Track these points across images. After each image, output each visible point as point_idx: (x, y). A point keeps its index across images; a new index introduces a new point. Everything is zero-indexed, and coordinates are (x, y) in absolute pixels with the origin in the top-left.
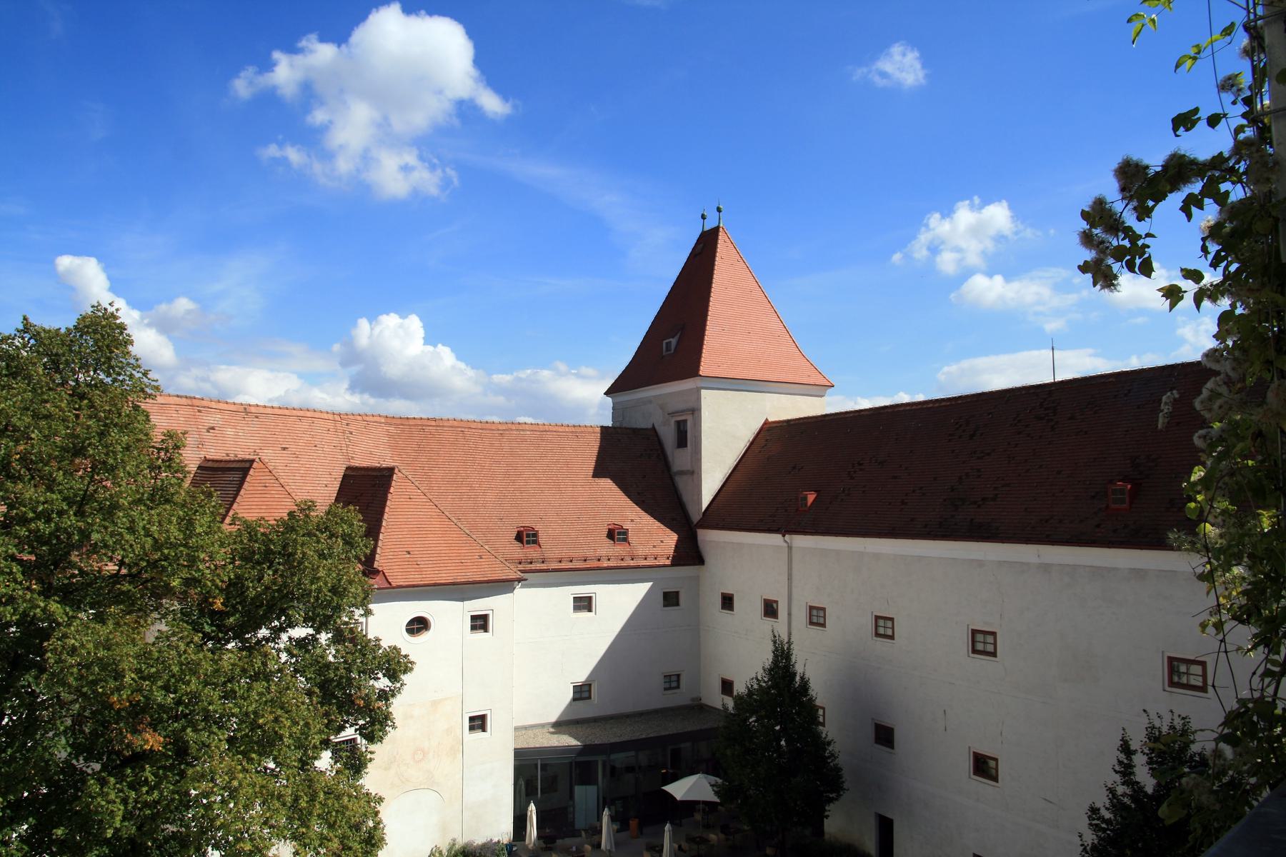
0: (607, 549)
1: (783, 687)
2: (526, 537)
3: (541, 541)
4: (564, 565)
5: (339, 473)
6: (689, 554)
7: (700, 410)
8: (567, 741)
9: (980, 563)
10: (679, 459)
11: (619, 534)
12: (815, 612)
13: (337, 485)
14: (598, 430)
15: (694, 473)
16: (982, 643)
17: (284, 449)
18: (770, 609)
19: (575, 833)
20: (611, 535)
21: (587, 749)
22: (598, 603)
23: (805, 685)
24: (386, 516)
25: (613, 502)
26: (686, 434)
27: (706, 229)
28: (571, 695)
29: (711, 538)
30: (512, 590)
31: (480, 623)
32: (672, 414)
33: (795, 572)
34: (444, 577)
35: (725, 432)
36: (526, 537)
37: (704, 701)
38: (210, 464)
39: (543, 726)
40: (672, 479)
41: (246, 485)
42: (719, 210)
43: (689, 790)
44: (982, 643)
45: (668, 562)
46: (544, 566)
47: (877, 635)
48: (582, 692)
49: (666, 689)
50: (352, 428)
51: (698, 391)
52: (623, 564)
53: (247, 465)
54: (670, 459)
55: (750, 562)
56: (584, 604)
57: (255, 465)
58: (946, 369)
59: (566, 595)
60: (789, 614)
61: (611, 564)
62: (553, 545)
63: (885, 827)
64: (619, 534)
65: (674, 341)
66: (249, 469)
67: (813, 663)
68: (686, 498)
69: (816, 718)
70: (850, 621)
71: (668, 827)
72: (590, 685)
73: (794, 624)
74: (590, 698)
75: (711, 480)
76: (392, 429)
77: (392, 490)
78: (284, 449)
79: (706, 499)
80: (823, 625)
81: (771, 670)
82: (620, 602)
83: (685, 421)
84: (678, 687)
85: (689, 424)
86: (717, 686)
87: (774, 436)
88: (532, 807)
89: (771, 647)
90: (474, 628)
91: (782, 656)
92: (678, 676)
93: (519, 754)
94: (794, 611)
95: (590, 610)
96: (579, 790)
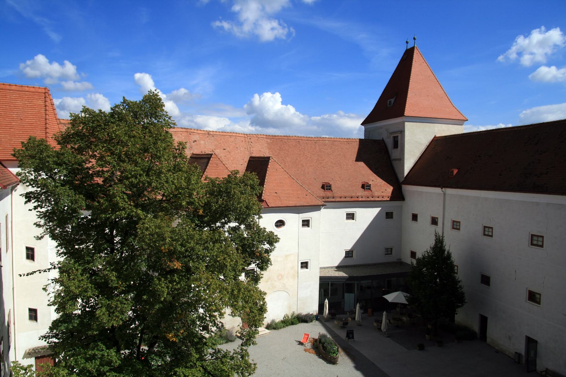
0: (362, 193)
1: (439, 255)
2: (326, 187)
3: (333, 189)
4: (342, 199)
5: (247, 159)
6: (398, 195)
8: (341, 274)
9: (537, 204)
10: (394, 154)
11: (367, 186)
14: (358, 140)
15: (401, 160)
17: (224, 149)
18: (434, 221)
19: (344, 313)
20: (363, 187)
21: (350, 278)
22: (357, 216)
23: (449, 255)
24: (266, 177)
25: (364, 172)
26: (398, 141)
27: (409, 48)
29: (408, 189)
30: (319, 210)
31: (306, 223)
33: (446, 205)
34: (291, 203)
35: (416, 141)
36: (326, 187)
38: (194, 156)
39: (332, 267)
40: (391, 163)
41: (209, 164)
42: (414, 39)
45: (388, 199)
46: (333, 200)
47: (484, 235)
48: (349, 254)
49: (386, 254)
50: (252, 140)
55: (426, 200)
56: (351, 216)
57: (213, 156)
59: (343, 212)
60: (443, 224)
61: (363, 199)
62: (338, 191)
63: (484, 321)
64: (367, 186)
65: (393, 100)
66: (210, 158)
67: (454, 246)
68: (397, 171)
70: (471, 227)
71: (385, 313)
75: (409, 164)
76: (269, 140)
77: (269, 166)
78: (224, 149)
79: (407, 171)
80: (459, 229)
81: (434, 248)
82: (366, 216)
83: (397, 137)
84: (391, 254)
85: (399, 138)
86: (409, 254)
87: (438, 144)
88: (327, 301)
89: (434, 238)
90: (303, 225)
93: (321, 278)
94: (445, 223)
95: (353, 219)
96: (346, 295)
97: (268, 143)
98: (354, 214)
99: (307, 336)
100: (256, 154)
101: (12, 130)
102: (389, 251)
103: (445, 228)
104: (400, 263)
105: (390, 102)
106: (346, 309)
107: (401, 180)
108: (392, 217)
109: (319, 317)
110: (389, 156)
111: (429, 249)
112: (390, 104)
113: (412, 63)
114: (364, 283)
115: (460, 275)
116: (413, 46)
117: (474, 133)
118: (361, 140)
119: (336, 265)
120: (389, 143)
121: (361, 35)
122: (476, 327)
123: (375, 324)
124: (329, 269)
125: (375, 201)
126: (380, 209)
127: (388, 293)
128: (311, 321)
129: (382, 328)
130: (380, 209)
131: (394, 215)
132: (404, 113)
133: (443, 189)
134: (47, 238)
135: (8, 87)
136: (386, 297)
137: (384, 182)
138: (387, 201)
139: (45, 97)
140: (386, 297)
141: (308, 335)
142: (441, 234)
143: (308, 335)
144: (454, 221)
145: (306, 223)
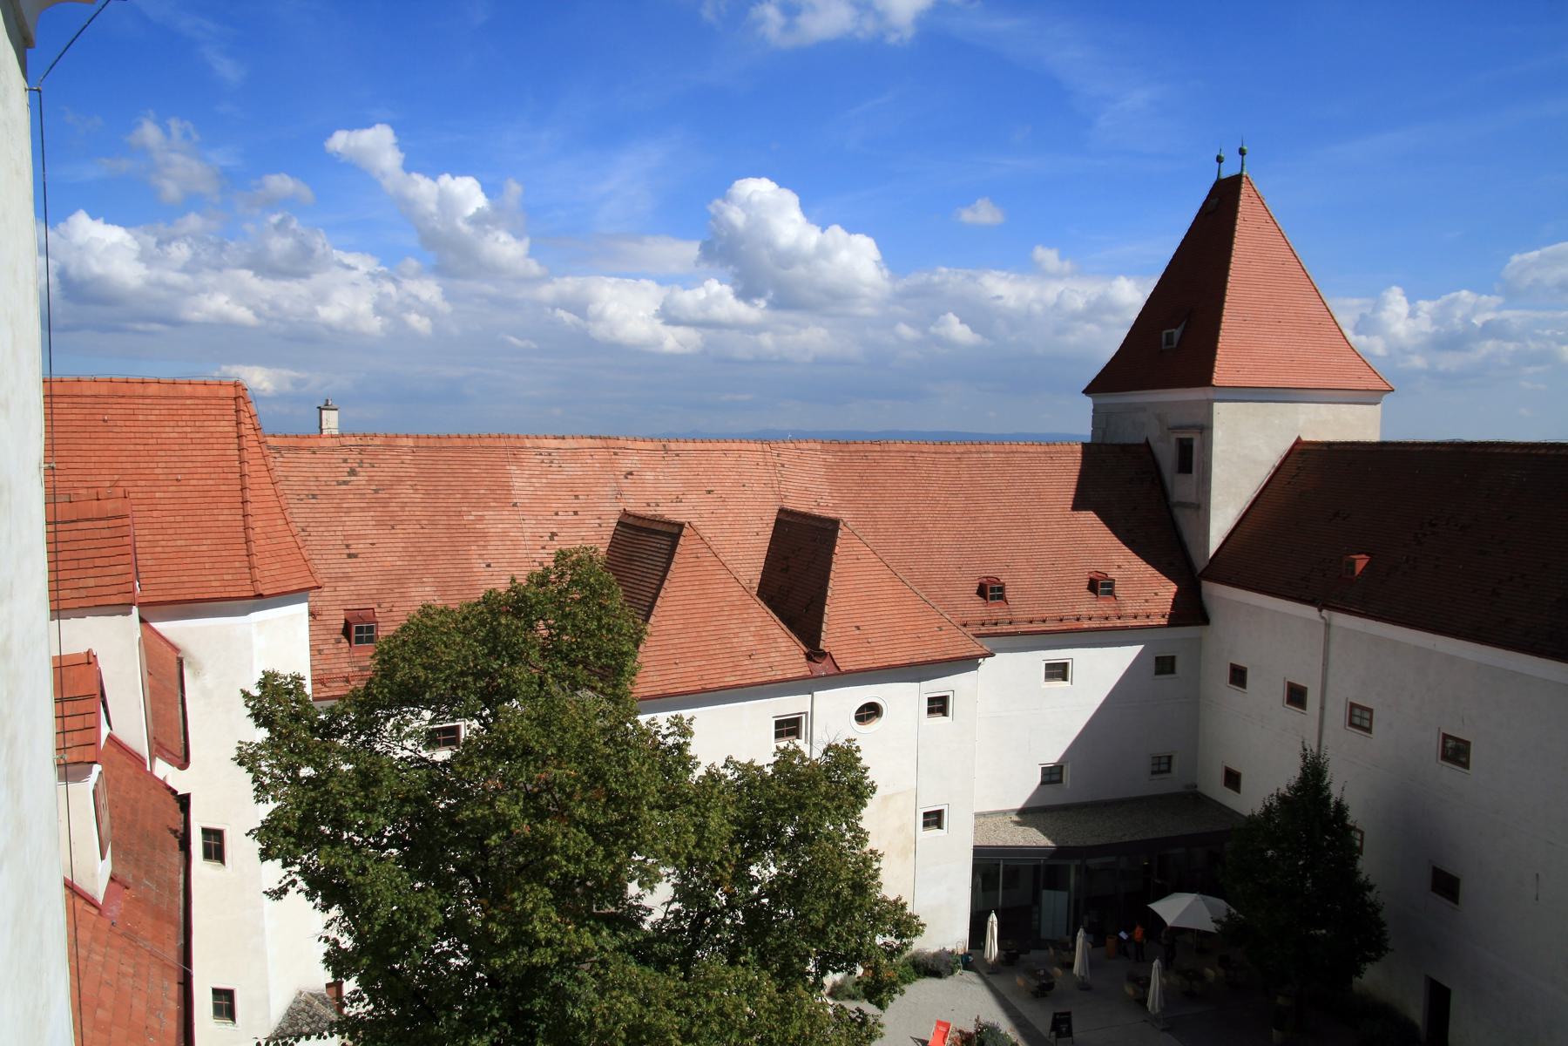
0: (1089, 608)
1: (1310, 803)
2: (990, 591)
3: (1008, 595)
5: (771, 517)
6: (1190, 610)
7: (1210, 428)
8: (1034, 838)
10: (1180, 488)
11: (1103, 585)
12: (1357, 712)
14: (1079, 448)
15: (1201, 508)
17: (709, 492)
18: (1296, 696)
19: (1041, 944)
20: (1093, 586)
21: (1061, 852)
22: (1075, 671)
23: (1341, 809)
24: (831, 584)
26: (1192, 453)
27: (1224, 175)
28: (1039, 780)
29: (1218, 594)
30: (976, 666)
31: (938, 706)
33: (1332, 656)
34: (900, 657)
35: (1243, 451)
36: (990, 591)
37: (1201, 789)
38: (630, 521)
39: (1004, 813)
40: (1170, 513)
41: (676, 558)
42: (1242, 152)
43: (1181, 916)
45: (1164, 622)
46: (1011, 628)
48: (1051, 775)
49: (1153, 773)
50: (784, 459)
51: (1209, 404)
53: (676, 530)
54: (1169, 486)
55: (1269, 632)
56: (1058, 671)
57: (685, 532)
58: (1516, 258)
59: (1038, 660)
60: (1322, 708)
61: (1094, 624)
62: (1021, 605)
63: (1439, 998)
64: (1103, 585)
65: (1177, 333)
66: (679, 535)
67: (1347, 784)
68: (1188, 535)
69: (1352, 846)
70: (1405, 731)
71: (1156, 963)
74: (1060, 781)
75: (1221, 521)
76: (829, 457)
77: (837, 550)
78: (709, 492)
79: (1215, 540)
80: (1369, 730)
82: (1102, 669)
83: (1191, 440)
84: (1169, 771)
85: (1196, 444)
86: (1220, 776)
87: (1306, 462)
88: (993, 918)
89: (1299, 762)
90: (931, 711)
91: (1313, 773)
92: (1170, 758)
93: (978, 852)
94: (1329, 706)
95: (1065, 679)
96: (1046, 895)
97: (829, 467)
99: (943, 1029)
101: (155, 514)
102: (1162, 765)
103: (1326, 732)
104: (1193, 799)
105: (1169, 336)
106: (1045, 933)
107: (1200, 565)
108: (1172, 671)
109: (970, 960)
110: (1164, 494)
113: (1234, 224)
114: (1093, 862)
115: (1367, 866)
116: (1236, 171)
117: (1414, 444)
119: (1019, 805)
120: (1167, 455)
122: (1416, 1011)
123: (1129, 989)
124: (997, 819)
125: (1126, 628)
126: (1140, 647)
127: (1161, 894)
128: (952, 973)
129: (1149, 1005)
130: (1140, 647)
131: (1179, 665)
132: (1211, 378)
133: (1325, 613)
134: (296, 900)
135: (139, 389)
136: (1158, 907)
137: (1152, 570)
139: (237, 411)
140: (1158, 907)
141: (947, 1025)
142: (1312, 745)
143: (947, 1025)
144: (1353, 706)
145: (938, 706)
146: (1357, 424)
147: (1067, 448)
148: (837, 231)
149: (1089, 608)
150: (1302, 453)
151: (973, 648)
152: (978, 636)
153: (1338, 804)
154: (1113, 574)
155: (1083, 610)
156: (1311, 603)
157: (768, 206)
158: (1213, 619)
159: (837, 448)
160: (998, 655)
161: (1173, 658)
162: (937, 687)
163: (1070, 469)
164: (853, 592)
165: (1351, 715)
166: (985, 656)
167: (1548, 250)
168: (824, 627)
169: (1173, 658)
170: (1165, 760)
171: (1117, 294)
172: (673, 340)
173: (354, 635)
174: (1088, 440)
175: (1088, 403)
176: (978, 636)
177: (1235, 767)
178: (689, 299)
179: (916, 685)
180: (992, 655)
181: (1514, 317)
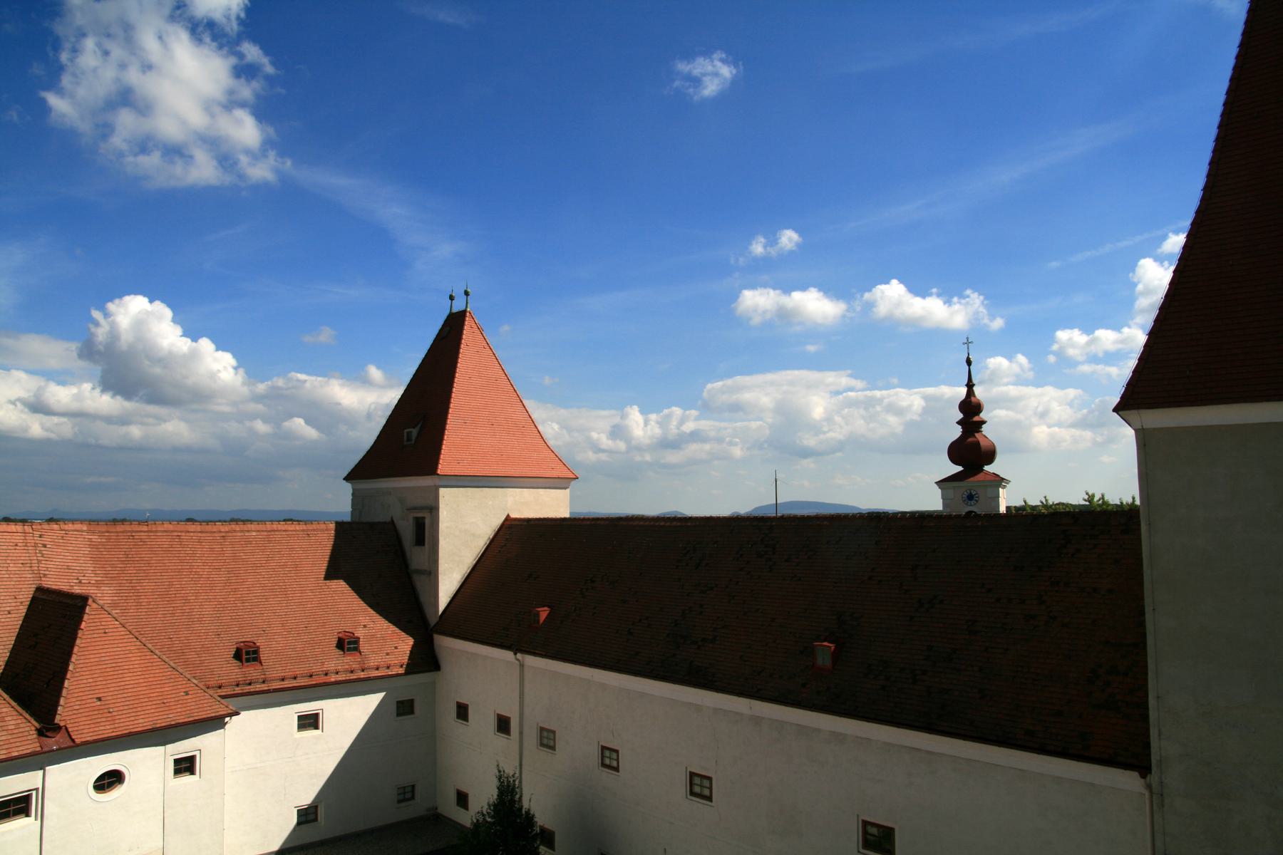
0: (338, 663)
2: (246, 654)
4: (287, 684)
5: (26, 595)
6: (425, 660)
7: (437, 509)
9: (698, 708)
10: (417, 558)
11: (349, 643)
13: (23, 610)
14: (333, 526)
15: (431, 573)
16: (699, 786)
18: (503, 725)
20: (341, 645)
22: (327, 720)
24: (74, 658)
25: (347, 608)
26: (425, 529)
27: (455, 310)
28: (295, 821)
29: (448, 645)
31: (185, 766)
32: (415, 508)
33: (526, 690)
34: (142, 723)
35: (464, 528)
36: (246, 654)
37: (440, 810)
42: (467, 293)
44: (699, 786)
45: (402, 671)
46: (264, 687)
47: (604, 765)
48: (306, 816)
49: (400, 801)
50: (46, 540)
51: (436, 489)
52: (353, 677)
55: (484, 674)
56: (309, 722)
58: (709, 386)
60: (521, 733)
61: (340, 677)
62: (274, 666)
64: (349, 643)
65: (415, 432)
66: (83, 608)
67: (539, 800)
68: (424, 598)
70: (578, 748)
72: (316, 807)
73: (525, 745)
74: (316, 820)
75: (448, 583)
76: (95, 538)
77: (83, 625)
79: (444, 600)
81: (495, 805)
82: (348, 717)
85: (427, 522)
86: (453, 797)
87: (515, 537)
89: (495, 783)
91: (508, 793)
92: (413, 786)
95: (317, 728)
97: (92, 545)
98: (317, 715)
100: (54, 582)
102: (407, 794)
104: (435, 819)
107: (433, 621)
108: (412, 712)
111: (486, 807)
112: (409, 439)
113: (458, 348)
116: (463, 308)
118: (340, 526)
120: (406, 530)
121: (392, 208)
125: (369, 679)
131: (417, 706)
133: (519, 655)
137: (393, 628)
138: (398, 675)
142: (510, 769)
146: (551, 504)
147: (323, 526)
148: (206, 344)
149: (338, 663)
150: (510, 527)
151: (213, 708)
152: (224, 697)
153: (528, 812)
154: (360, 633)
155: (331, 666)
156: (508, 648)
157: (140, 318)
158: (443, 664)
159: (104, 528)
160: (244, 714)
161: (412, 701)
162: (183, 748)
163: (325, 541)
164: (98, 669)
165: (541, 737)
166: (231, 715)
167: (729, 382)
168: (62, 701)
169: (412, 701)
170: (409, 789)
171: (367, 398)
172: (36, 427)
173: (244, 657)
174: (348, 519)
175: (348, 488)
176: (224, 697)
177: (464, 789)
178: (61, 395)
179: (161, 749)
180: (237, 714)
181: (705, 425)
